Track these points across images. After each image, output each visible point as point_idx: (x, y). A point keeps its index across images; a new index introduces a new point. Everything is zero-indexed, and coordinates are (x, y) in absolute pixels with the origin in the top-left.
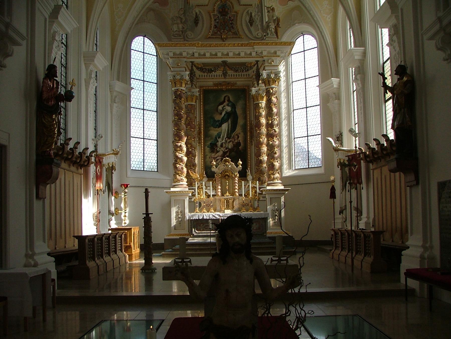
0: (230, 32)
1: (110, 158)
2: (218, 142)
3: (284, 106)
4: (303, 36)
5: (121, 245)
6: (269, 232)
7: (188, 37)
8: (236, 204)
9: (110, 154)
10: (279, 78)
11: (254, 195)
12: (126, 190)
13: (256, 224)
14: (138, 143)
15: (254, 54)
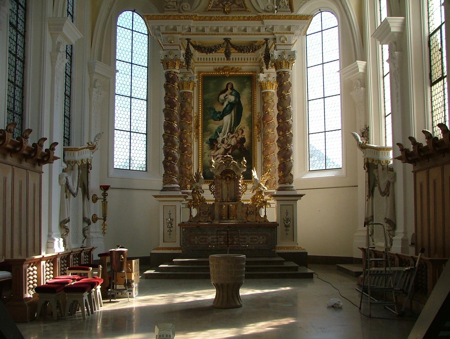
0: (235, 4)
2: (219, 137)
4: (321, 13)
6: (279, 247)
9: (84, 148)
13: (263, 237)
14: (124, 136)
15: (263, 30)
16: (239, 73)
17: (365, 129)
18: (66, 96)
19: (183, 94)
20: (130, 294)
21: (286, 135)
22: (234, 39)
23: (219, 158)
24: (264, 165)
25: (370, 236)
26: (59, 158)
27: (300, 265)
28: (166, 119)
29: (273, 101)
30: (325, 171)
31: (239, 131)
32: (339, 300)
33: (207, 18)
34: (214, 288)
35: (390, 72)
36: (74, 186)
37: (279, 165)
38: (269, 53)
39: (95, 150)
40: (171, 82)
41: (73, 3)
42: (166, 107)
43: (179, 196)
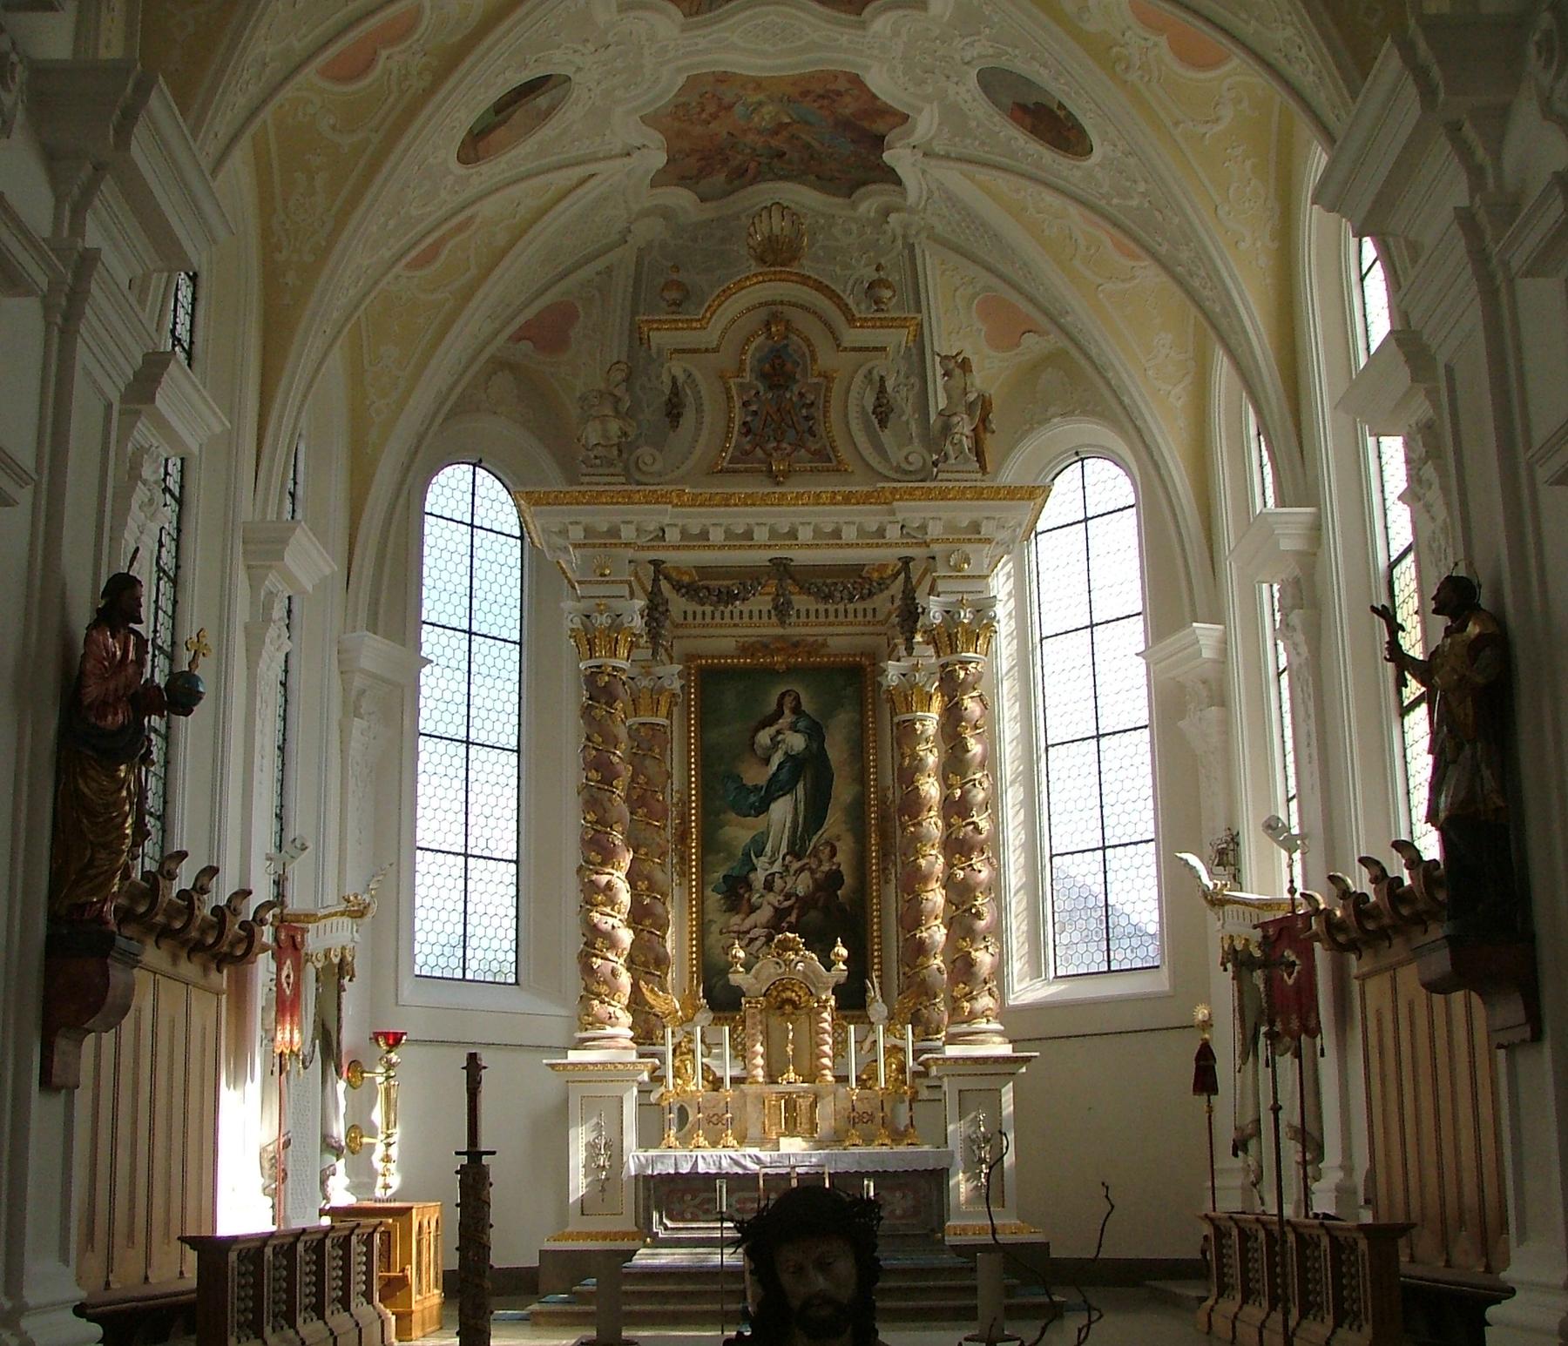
3: (1009, 729)
5: (369, 1273)
7: (644, 468)
8: (825, 1124)
9: (335, 914)
10: (989, 626)
11: (896, 1080)
12: (394, 1057)
14: (445, 871)
15: (893, 533)
19: (637, 729)
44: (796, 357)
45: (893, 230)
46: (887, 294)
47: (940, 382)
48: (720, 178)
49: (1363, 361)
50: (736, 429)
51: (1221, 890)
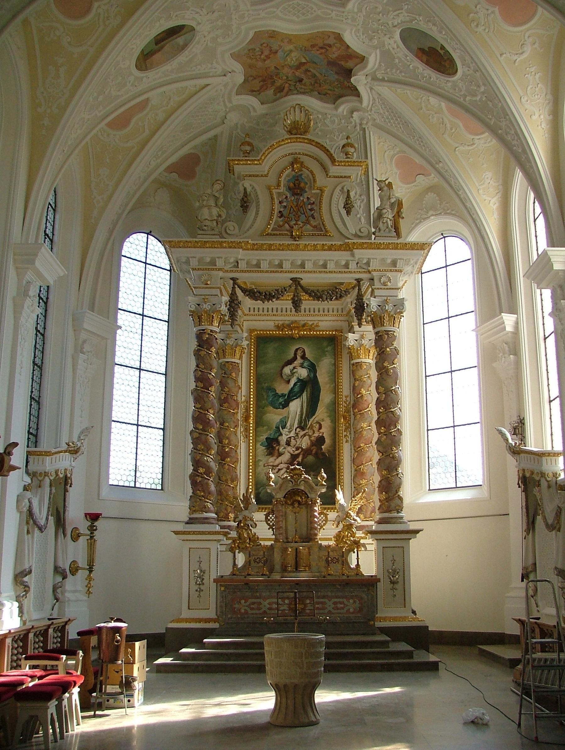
1: (61, 460)
2: (282, 435)
4: (443, 239)
6: (380, 617)
9: (61, 452)
13: (355, 602)
15: (353, 266)
16: (315, 333)
17: (518, 423)
18: (35, 366)
20: (129, 701)
21: (391, 432)
22: (307, 279)
23: (282, 469)
24: (355, 480)
25: (532, 597)
26: (20, 468)
27: (416, 648)
28: (196, 405)
29: (368, 377)
30: (456, 490)
31: (314, 425)
32: (482, 711)
33: (265, 246)
34: (271, 690)
35: (555, 332)
36: (41, 514)
37: (380, 482)
38: (362, 302)
39: (78, 454)
40: (205, 347)
41: (54, 221)
42: (196, 386)
43: (216, 532)
44: (306, 180)
45: (355, 121)
46: (352, 150)
47: (377, 193)
48: (270, 92)
49: (535, 257)
50: (276, 213)
51: (519, 445)
